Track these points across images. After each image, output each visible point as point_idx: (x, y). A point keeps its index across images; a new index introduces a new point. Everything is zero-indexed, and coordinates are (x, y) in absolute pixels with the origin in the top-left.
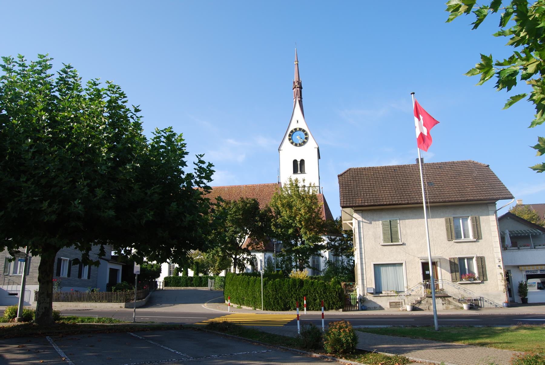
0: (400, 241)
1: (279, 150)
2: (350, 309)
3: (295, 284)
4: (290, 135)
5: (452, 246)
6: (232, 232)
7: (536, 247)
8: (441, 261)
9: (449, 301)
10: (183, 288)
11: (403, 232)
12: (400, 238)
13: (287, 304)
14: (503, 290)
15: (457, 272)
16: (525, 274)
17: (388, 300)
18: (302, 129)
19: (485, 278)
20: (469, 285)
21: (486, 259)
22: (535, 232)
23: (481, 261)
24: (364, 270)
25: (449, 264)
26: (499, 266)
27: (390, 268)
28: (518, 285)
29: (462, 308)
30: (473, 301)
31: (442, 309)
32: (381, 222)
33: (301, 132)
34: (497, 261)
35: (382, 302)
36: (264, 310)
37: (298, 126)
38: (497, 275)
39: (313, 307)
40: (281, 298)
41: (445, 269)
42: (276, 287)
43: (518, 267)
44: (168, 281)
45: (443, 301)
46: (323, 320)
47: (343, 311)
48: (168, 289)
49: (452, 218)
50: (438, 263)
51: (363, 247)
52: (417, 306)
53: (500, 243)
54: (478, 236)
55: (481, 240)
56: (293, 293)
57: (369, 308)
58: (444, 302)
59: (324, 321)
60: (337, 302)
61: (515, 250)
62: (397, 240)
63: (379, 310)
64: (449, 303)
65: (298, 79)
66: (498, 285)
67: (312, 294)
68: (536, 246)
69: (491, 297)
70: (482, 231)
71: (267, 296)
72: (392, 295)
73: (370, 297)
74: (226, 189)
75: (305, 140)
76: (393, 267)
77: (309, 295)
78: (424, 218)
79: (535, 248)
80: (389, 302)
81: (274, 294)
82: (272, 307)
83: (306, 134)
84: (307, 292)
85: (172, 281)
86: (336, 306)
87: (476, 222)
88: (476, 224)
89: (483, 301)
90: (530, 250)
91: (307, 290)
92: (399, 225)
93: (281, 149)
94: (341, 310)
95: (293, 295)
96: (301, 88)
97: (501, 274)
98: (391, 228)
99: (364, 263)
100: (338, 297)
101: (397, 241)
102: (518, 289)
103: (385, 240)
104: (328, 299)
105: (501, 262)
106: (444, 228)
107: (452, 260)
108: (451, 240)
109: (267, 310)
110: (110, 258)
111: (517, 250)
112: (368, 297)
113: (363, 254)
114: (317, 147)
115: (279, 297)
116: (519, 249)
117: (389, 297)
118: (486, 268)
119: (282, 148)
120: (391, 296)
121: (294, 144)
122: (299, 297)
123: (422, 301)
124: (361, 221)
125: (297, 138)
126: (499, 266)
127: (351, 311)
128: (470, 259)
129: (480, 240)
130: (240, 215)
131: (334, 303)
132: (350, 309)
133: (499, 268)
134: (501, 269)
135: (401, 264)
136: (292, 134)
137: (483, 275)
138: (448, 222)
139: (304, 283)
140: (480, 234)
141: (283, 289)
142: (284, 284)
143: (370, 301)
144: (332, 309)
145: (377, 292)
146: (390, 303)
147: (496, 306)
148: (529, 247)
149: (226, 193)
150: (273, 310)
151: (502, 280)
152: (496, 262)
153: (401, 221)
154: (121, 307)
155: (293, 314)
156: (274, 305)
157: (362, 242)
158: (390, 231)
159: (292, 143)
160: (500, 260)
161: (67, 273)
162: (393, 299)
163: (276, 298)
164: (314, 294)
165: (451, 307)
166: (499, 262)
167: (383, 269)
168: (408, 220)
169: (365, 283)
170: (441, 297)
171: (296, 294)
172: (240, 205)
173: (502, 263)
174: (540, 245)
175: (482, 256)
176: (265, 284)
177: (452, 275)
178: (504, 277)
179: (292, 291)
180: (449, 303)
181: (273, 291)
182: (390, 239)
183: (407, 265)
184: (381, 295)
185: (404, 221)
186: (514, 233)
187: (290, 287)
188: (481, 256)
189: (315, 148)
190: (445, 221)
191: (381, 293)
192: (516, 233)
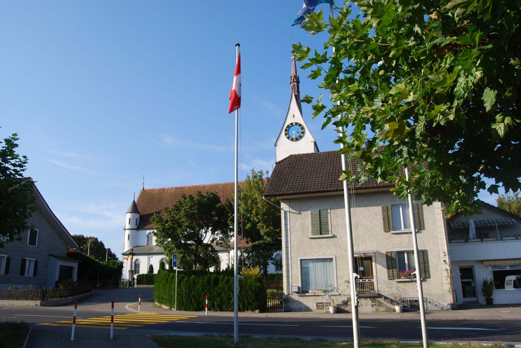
0: (330, 233)
1: (275, 145)
2: (277, 311)
3: (210, 281)
4: (286, 130)
5: (390, 238)
6: (185, 227)
7: (503, 239)
8: (376, 255)
9: (380, 303)
10: (145, 286)
11: (334, 223)
12: (330, 229)
13: (200, 303)
14: (448, 289)
15: (395, 268)
16: (491, 270)
17: (314, 300)
18: (298, 123)
19: (427, 276)
20: (408, 284)
21: (429, 253)
22: (507, 222)
23: (423, 255)
24: (290, 266)
25: (386, 260)
26: (445, 261)
27: (320, 265)
28: (482, 282)
29: (394, 310)
30: (407, 302)
31: (371, 312)
32: (309, 212)
33: (298, 127)
34: (442, 255)
35: (308, 302)
36: (177, 310)
37: (293, 121)
38: (441, 272)
39: (227, 307)
40: (194, 297)
41: (380, 264)
42: (189, 285)
43: (482, 261)
44: (140, 279)
45: (373, 302)
46: (74, 326)
47: (259, 312)
48: (140, 287)
49: (389, 206)
50: (373, 258)
51: (289, 240)
52: (343, 307)
53: (445, 234)
54: (420, 226)
55: (424, 230)
56: (206, 291)
57: (293, 309)
58: (373, 304)
59: (76, 328)
60: (253, 302)
61: (477, 243)
62: (327, 232)
63: (305, 311)
64: (380, 304)
65: (295, 73)
66: (443, 283)
67: (227, 292)
68: (503, 237)
69: (434, 298)
70: (425, 220)
71: (180, 294)
72: (319, 294)
73: (295, 297)
74: (220, 186)
75: (302, 135)
76: (323, 263)
77: (223, 294)
78: (344, 207)
79: (501, 240)
80: (316, 303)
81: (187, 293)
82: (185, 307)
83: (303, 128)
84: (221, 291)
85: (144, 279)
86: (252, 307)
87: (418, 210)
88: (418, 212)
89: (427, 302)
90: (495, 241)
91: (221, 289)
92: (329, 215)
93: (278, 144)
94: (257, 311)
95: (207, 294)
96: (298, 82)
97: (447, 270)
98: (320, 218)
99: (290, 258)
100: (254, 296)
101: (328, 233)
102: (482, 287)
103: (313, 233)
104: (243, 298)
105: (447, 256)
106: (380, 217)
107: (389, 255)
108: (388, 231)
109: (180, 310)
110: (65, 255)
111: (480, 242)
112: (292, 297)
113: (289, 249)
114: (314, 141)
115: (192, 295)
116: (482, 241)
117: (317, 297)
118: (428, 263)
119: (278, 144)
120: (318, 296)
121: (290, 138)
122: (213, 297)
123: (349, 302)
124: (288, 211)
125: (294, 133)
126: (445, 261)
127: (278, 312)
128: (410, 253)
129: (422, 231)
130: (195, 209)
131: (249, 303)
132: (277, 311)
133: (444, 263)
134: (447, 264)
135: (331, 260)
136: (288, 129)
137: (425, 272)
138: (385, 210)
139: (220, 280)
140: (422, 224)
141: (197, 287)
142: (198, 281)
143: (297, 302)
144: (248, 310)
145: (303, 291)
146: (317, 303)
147: (442, 308)
148: (495, 239)
149: (221, 190)
150: (185, 310)
151: (447, 277)
152: (441, 256)
153: (332, 211)
154: (37, 305)
155: (188, 314)
156: (187, 304)
157: (289, 235)
158: (319, 222)
159: (288, 138)
160: (445, 254)
161: (33, 273)
162: (320, 300)
163: (189, 297)
164: (228, 293)
165: (382, 309)
166: (445, 256)
167: (311, 265)
168: (340, 209)
169: (290, 281)
170: (370, 297)
171: (209, 293)
172: (196, 198)
173: (447, 258)
174: (508, 237)
175: (424, 249)
176: (179, 282)
177: (388, 272)
178: (449, 273)
179: (206, 289)
180: (380, 304)
181: (187, 289)
182: (319, 231)
183: (337, 260)
184: (307, 294)
185: (335, 210)
186: (483, 223)
187: (204, 285)
188: (423, 249)
189: (312, 142)
190: (381, 209)
191: (308, 292)
192: (485, 223)
